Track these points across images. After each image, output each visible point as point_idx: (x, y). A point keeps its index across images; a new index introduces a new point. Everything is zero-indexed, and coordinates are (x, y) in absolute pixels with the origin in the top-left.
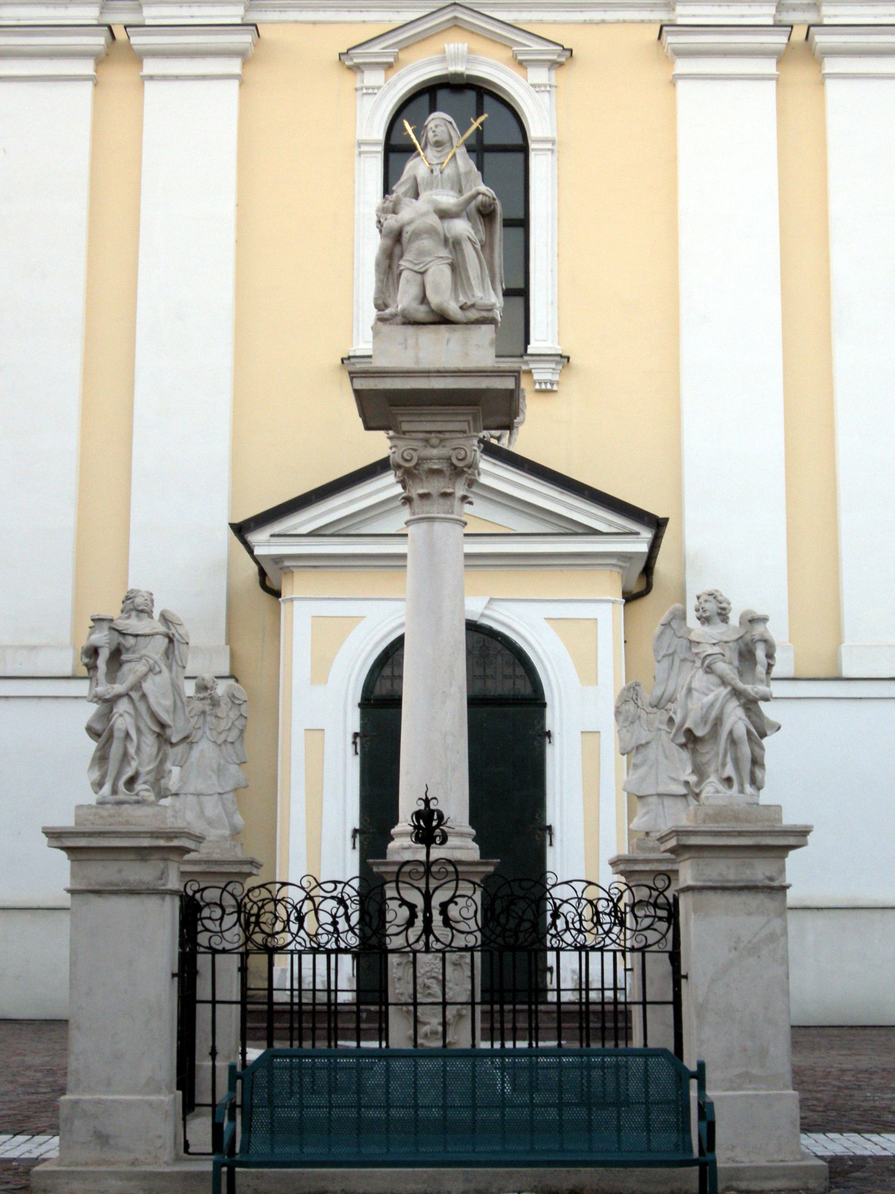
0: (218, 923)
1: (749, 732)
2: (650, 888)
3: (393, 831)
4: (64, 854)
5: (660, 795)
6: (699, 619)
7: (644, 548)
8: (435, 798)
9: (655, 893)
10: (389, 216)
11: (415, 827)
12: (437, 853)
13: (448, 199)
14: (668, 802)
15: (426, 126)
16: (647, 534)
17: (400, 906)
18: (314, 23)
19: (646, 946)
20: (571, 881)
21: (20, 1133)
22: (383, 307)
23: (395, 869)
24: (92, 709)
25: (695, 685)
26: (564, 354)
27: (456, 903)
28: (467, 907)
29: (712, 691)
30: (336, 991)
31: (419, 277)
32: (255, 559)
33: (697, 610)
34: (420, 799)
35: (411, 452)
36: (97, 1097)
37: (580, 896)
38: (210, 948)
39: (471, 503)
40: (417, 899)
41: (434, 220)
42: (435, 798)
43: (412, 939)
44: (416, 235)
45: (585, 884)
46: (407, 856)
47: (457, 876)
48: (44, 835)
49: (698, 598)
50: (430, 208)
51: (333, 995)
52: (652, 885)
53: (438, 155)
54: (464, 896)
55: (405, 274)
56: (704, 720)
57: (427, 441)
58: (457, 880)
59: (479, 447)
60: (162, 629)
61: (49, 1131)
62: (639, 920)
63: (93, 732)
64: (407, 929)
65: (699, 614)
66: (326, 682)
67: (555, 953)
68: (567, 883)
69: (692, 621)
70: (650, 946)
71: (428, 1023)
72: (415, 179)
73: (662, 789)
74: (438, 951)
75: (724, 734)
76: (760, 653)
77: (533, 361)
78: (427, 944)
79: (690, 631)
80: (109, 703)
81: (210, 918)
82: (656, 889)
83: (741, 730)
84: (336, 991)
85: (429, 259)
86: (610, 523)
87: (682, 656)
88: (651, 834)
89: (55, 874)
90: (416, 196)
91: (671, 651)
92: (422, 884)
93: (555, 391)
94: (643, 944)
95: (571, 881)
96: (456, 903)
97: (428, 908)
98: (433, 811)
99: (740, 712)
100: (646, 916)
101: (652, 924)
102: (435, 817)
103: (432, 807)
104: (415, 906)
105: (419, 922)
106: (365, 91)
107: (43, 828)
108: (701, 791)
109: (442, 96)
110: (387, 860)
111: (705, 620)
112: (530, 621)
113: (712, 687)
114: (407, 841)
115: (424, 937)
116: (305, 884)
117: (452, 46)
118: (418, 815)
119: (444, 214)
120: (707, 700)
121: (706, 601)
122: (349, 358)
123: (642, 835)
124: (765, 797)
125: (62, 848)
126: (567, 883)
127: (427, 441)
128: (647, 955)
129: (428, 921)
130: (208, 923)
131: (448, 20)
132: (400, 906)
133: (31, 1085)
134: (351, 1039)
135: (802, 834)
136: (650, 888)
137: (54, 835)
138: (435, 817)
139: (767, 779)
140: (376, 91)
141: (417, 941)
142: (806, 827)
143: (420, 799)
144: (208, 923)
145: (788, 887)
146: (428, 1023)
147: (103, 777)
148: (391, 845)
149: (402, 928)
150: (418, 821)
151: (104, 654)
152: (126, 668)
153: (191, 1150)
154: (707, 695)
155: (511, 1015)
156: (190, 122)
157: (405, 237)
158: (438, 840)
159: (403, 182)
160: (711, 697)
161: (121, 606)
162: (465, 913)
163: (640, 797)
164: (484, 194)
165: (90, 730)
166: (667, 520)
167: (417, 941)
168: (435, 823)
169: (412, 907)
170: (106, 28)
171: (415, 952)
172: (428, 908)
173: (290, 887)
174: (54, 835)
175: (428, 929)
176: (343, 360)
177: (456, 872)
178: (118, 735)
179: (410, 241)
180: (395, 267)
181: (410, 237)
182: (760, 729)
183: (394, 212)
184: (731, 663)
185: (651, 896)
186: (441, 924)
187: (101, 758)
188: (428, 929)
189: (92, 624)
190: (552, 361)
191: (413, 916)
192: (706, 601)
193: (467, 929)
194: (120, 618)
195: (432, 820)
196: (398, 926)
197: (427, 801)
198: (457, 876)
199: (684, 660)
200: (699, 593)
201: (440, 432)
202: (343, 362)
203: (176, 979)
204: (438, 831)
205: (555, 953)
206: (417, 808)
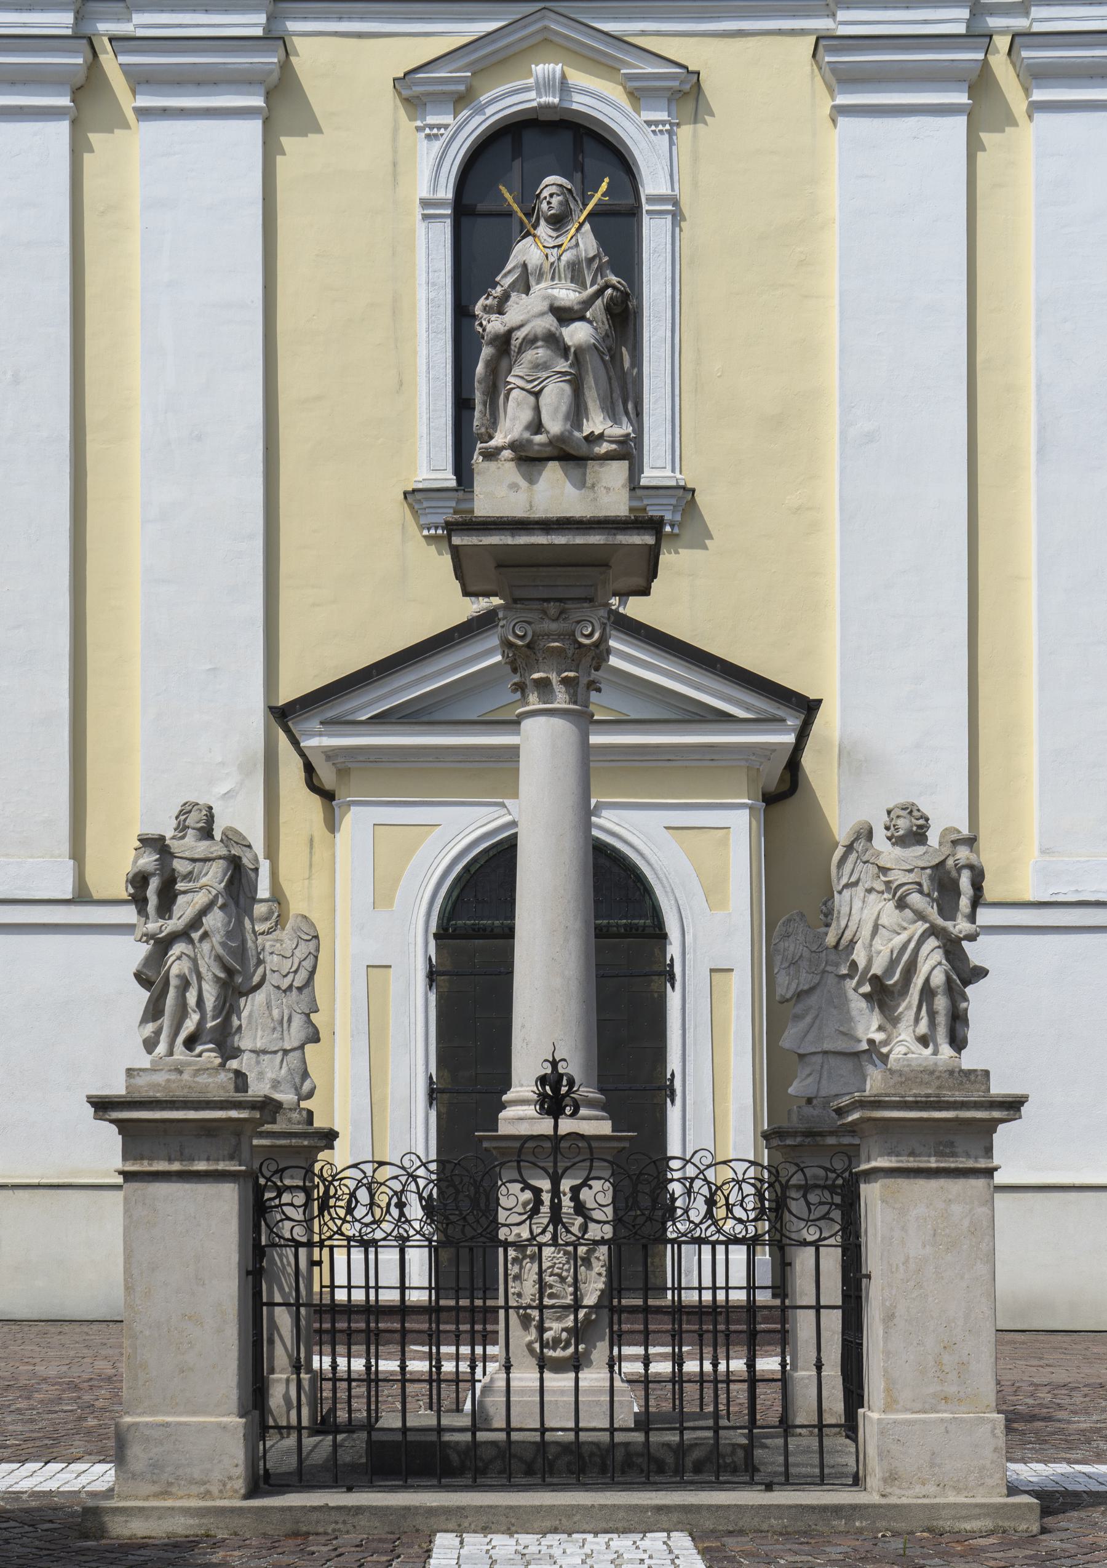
0: (301, 1210)
1: (949, 980)
2: (826, 1169)
3: (505, 1098)
4: (114, 1129)
5: (825, 1053)
6: (889, 838)
7: (790, 738)
8: (564, 1060)
9: (832, 1176)
10: (493, 317)
11: (539, 1095)
12: (567, 1126)
13: (567, 295)
14: (833, 1061)
15: (538, 196)
16: (794, 721)
17: (522, 1190)
18: (360, 35)
19: (820, 1240)
20: (730, 1161)
21: (54, 1459)
22: (487, 438)
23: (517, 1145)
24: (143, 950)
25: (883, 920)
26: (689, 486)
27: (590, 1187)
28: (604, 1191)
29: (905, 929)
30: (377, 1288)
31: (532, 399)
32: (302, 753)
33: (887, 828)
34: (546, 1060)
35: (525, 625)
36: (160, 1419)
37: (740, 1178)
38: (293, 1240)
39: (599, 690)
40: (545, 1184)
41: (549, 322)
42: (564, 1060)
43: (537, 1230)
44: (530, 341)
45: (747, 1164)
46: (524, 1129)
47: (592, 1153)
48: (89, 1105)
49: (889, 812)
50: (545, 306)
51: (372, 1292)
52: (829, 1166)
53: (554, 234)
54: (599, 1178)
55: (515, 393)
56: (893, 963)
57: (544, 612)
58: (592, 1161)
59: (609, 619)
60: (224, 852)
61: (88, 1457)
62: (812, 1207)
63: (142, 978)
64: (530, 1218)
65: (889, 834)
66: (391, 906)
67: (723, 1247)
68: (725, 1163)
69: (880, 840)
70: (825, 1239)
71: (551, 1329)
72: (525, 265)
73: (827, 1046)
74: (567, 1244)
75: (918, 982)
76: (965, 881)
77: (650, 497)
78: (555, 1237)
79: (878, 854)
80: (162, 945)
81: (292, 1205)
82: (834, 1171)
83: (938, 979)
84: (377, 1288)
85: (545, 375)
86: (747, 709)
87: (868, 885)
88: (815, 1102)
89: (103, 1150)
90: (527, 290)
91: (853, 879)
92: (549, 1165)
93: (677, 535)
94: (816, 1237)
95: (730, 1161)
96: (590, 1187)
97: (556, 1192)
98: (561, 1076)
99: (938, 956)
100: (821, 1203)
101: (828, 1213)
102: (565, 1082)
103: (561, 1071)
104: (541, 1190)
105: (545, 1209)
106: (427, 131)
107: (88, 1097)
108: (890, 1051)
109: (530, 138)
110: (500, 1133)
111: (901, 841)
112: (640, 830)
113: (905, 924)
114: (530, 1111)
115: (551, 1228)
116: (407, 1164)
117: (541, 66)
118: (543, 1080)
119: (564, 315)
120: (899, 940)
121: (898, 817)
122: (414, 491)
123: (803, 1102)
124: (969, 1060)
125: (112, 1121)
126: (725, 1163)
127: (544, 612)
128: (821, 1249)
129: (556, 1208)
130: (289, 1210)
131: (537, 32)
132: (522, 1190)
133: (51, 1401)
134: (423, 1345)
135: (1013, 1106)
136: (826, 1169)
137: (102, 1106)
138: (565, 1082)
139: (971, 1035)
140: (442, 131)
141: (543, 1232)
142: (1017, 1096)
143: (546, 1060)
144: (289, 1210)
145: (996, 1169)
146: (551, 1329)
147: (158, 1033)
148: (502, 1115)
149: (525, 1217)
150: (544, 1088)
151: (154, 884)
152: (181, 900)
153: (271, 1482)
154: (899, 934)
155: (481, 1315)
156: (185, 168)
157: (515, 343)
158: (568, 1111)
159: (509, 272)
160: (904, 937)
161: (174, 823)
162: (601, 1199)
163: (801, 1056)
164: (614, 287)
165: (138, 976)
166: (820, 701)
167: (543, 1232)
168: (564, 1090)
169: (537, 1192)
170: (85, 41)
171: (540, 1246)
172: (556, 1192)
173: (388, 1167)
174: (102, 1106)
175: (556, 1217)
176: (405, 494)
177: (590, 1148)
178: (174, 982)
179: (520, 351)
180: (501, 384)
181: (521, 344)
182: (964, 974)
183: (501, 312)
184: (928, 895)
185: (827, 1178)
186: (572, 1211)
187: (154, 1011)
188: (556, 1217)
189: (138, 844)
190: (672, 496)
191: (538, 1202)
192: (898, 817)
193: (604, 1218)
194: (173, 838)
195: (561, 1085)
196: (520, 1214)
197: (554, 1064)
198: (592, 1153)
199: (870, 891)
200: (891, 806)
201: (560, 600)
202: (405, 498)
203: (250, 1277)
204: (567, 1100)
205: (723, 1247)
206: (543, 1072)
